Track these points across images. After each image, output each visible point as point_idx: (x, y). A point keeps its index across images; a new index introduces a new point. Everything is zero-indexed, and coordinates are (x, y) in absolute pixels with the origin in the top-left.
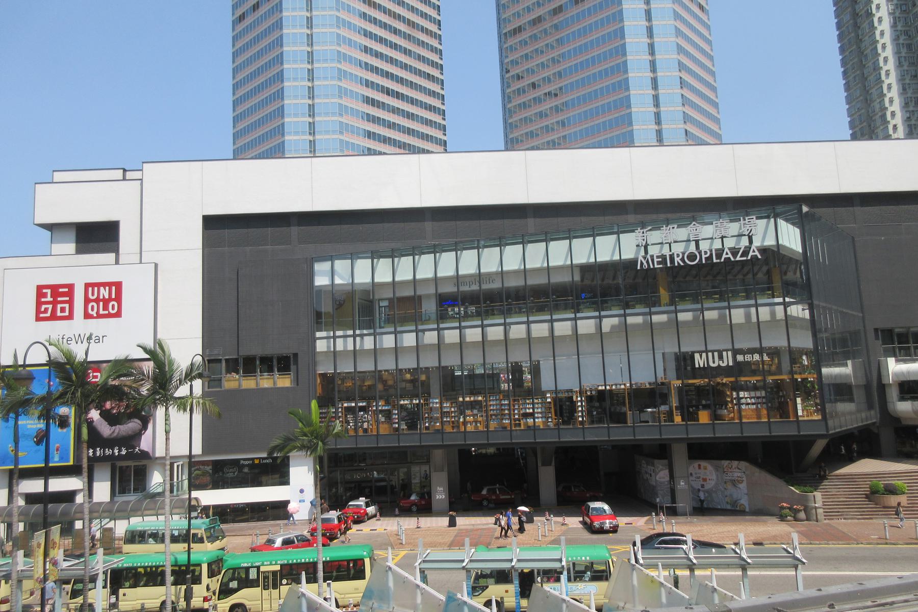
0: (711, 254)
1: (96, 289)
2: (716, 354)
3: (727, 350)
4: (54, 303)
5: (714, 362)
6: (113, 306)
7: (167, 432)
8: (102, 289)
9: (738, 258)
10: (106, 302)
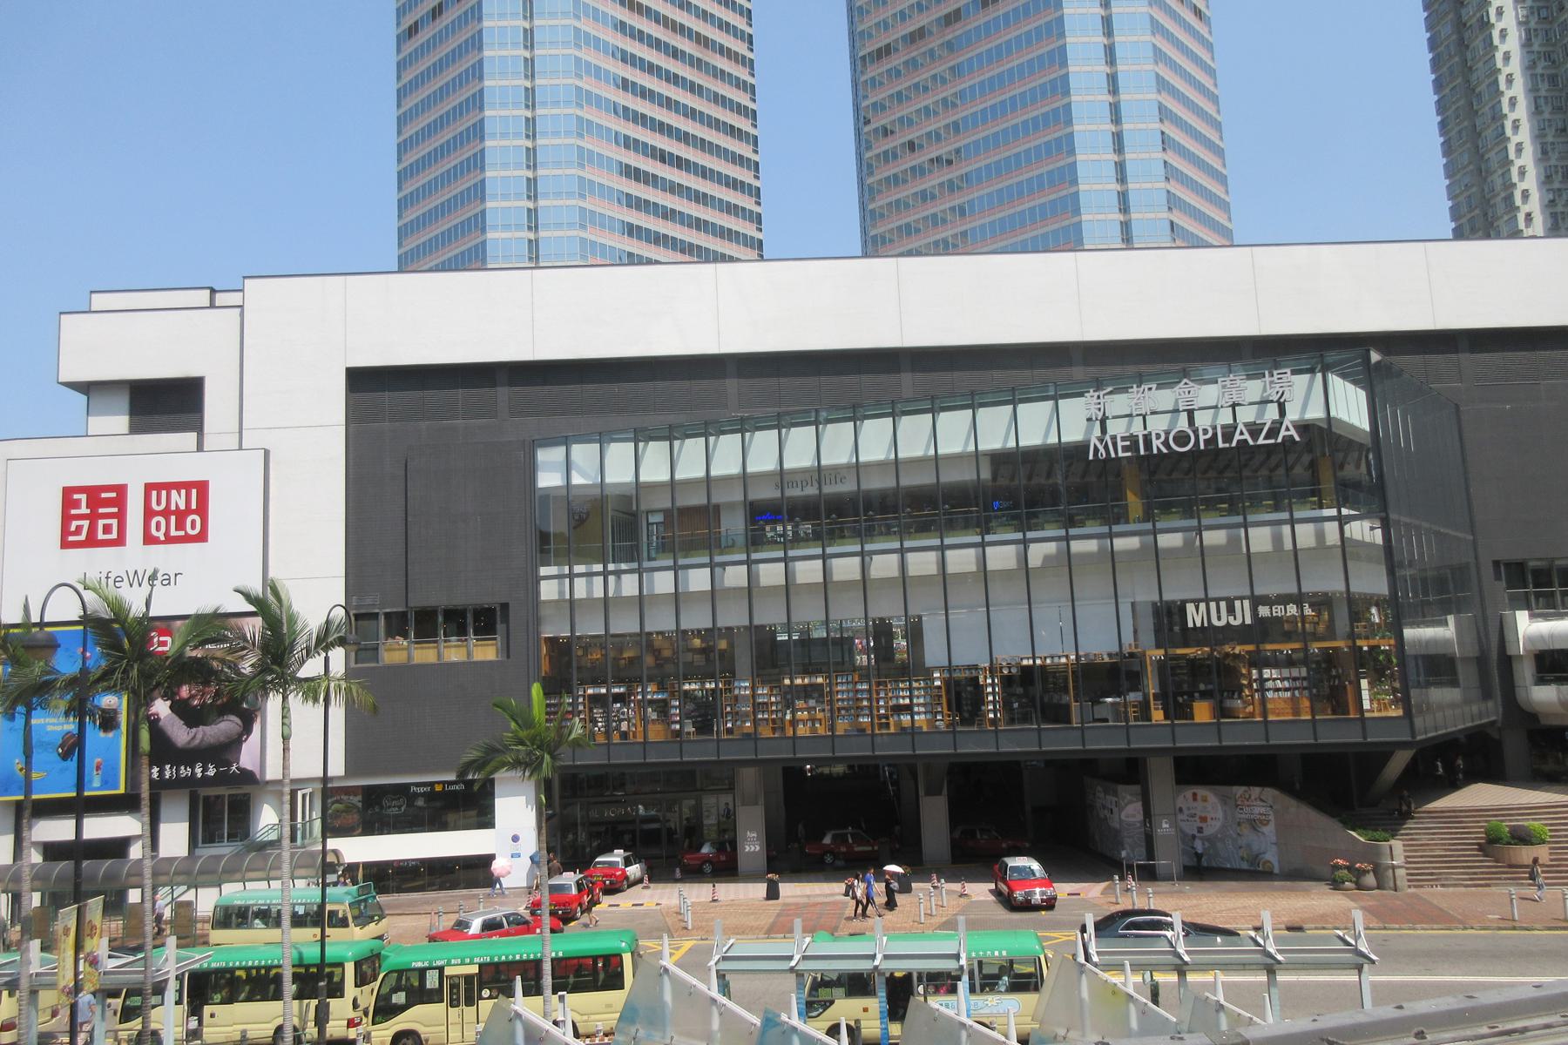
0: (1215, 434)
1: (164, 493)
2: (1223, 604)
3: (1242, 598)
4: (93, 518)
5: (1219, 618)
6: (193, 522)
7: (286, 738)
8: (174, 493)
9: (1261, 441)
10: (181, 516)
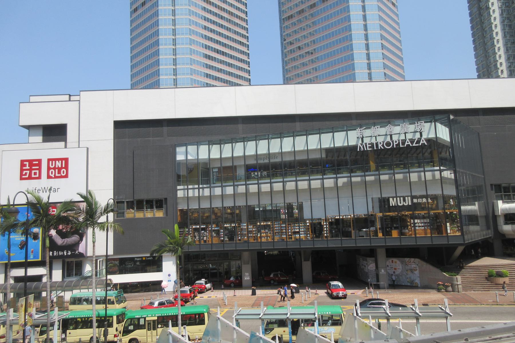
0: (399, 143)
1: (54, 162)
2: (402, 198)
3: (408, 196)
4: (31, 170)
5: (400, 203)
6: (63, 171)
7: (94, 242)
8: (57, 162)
9: (414, 145)
10: (60, 169)
